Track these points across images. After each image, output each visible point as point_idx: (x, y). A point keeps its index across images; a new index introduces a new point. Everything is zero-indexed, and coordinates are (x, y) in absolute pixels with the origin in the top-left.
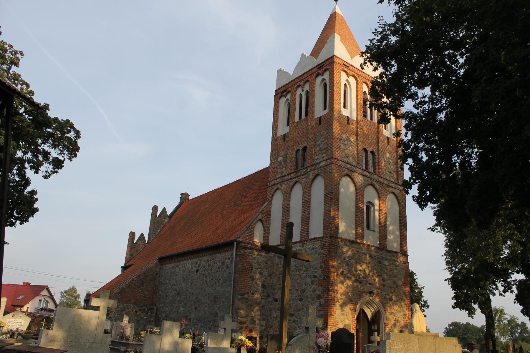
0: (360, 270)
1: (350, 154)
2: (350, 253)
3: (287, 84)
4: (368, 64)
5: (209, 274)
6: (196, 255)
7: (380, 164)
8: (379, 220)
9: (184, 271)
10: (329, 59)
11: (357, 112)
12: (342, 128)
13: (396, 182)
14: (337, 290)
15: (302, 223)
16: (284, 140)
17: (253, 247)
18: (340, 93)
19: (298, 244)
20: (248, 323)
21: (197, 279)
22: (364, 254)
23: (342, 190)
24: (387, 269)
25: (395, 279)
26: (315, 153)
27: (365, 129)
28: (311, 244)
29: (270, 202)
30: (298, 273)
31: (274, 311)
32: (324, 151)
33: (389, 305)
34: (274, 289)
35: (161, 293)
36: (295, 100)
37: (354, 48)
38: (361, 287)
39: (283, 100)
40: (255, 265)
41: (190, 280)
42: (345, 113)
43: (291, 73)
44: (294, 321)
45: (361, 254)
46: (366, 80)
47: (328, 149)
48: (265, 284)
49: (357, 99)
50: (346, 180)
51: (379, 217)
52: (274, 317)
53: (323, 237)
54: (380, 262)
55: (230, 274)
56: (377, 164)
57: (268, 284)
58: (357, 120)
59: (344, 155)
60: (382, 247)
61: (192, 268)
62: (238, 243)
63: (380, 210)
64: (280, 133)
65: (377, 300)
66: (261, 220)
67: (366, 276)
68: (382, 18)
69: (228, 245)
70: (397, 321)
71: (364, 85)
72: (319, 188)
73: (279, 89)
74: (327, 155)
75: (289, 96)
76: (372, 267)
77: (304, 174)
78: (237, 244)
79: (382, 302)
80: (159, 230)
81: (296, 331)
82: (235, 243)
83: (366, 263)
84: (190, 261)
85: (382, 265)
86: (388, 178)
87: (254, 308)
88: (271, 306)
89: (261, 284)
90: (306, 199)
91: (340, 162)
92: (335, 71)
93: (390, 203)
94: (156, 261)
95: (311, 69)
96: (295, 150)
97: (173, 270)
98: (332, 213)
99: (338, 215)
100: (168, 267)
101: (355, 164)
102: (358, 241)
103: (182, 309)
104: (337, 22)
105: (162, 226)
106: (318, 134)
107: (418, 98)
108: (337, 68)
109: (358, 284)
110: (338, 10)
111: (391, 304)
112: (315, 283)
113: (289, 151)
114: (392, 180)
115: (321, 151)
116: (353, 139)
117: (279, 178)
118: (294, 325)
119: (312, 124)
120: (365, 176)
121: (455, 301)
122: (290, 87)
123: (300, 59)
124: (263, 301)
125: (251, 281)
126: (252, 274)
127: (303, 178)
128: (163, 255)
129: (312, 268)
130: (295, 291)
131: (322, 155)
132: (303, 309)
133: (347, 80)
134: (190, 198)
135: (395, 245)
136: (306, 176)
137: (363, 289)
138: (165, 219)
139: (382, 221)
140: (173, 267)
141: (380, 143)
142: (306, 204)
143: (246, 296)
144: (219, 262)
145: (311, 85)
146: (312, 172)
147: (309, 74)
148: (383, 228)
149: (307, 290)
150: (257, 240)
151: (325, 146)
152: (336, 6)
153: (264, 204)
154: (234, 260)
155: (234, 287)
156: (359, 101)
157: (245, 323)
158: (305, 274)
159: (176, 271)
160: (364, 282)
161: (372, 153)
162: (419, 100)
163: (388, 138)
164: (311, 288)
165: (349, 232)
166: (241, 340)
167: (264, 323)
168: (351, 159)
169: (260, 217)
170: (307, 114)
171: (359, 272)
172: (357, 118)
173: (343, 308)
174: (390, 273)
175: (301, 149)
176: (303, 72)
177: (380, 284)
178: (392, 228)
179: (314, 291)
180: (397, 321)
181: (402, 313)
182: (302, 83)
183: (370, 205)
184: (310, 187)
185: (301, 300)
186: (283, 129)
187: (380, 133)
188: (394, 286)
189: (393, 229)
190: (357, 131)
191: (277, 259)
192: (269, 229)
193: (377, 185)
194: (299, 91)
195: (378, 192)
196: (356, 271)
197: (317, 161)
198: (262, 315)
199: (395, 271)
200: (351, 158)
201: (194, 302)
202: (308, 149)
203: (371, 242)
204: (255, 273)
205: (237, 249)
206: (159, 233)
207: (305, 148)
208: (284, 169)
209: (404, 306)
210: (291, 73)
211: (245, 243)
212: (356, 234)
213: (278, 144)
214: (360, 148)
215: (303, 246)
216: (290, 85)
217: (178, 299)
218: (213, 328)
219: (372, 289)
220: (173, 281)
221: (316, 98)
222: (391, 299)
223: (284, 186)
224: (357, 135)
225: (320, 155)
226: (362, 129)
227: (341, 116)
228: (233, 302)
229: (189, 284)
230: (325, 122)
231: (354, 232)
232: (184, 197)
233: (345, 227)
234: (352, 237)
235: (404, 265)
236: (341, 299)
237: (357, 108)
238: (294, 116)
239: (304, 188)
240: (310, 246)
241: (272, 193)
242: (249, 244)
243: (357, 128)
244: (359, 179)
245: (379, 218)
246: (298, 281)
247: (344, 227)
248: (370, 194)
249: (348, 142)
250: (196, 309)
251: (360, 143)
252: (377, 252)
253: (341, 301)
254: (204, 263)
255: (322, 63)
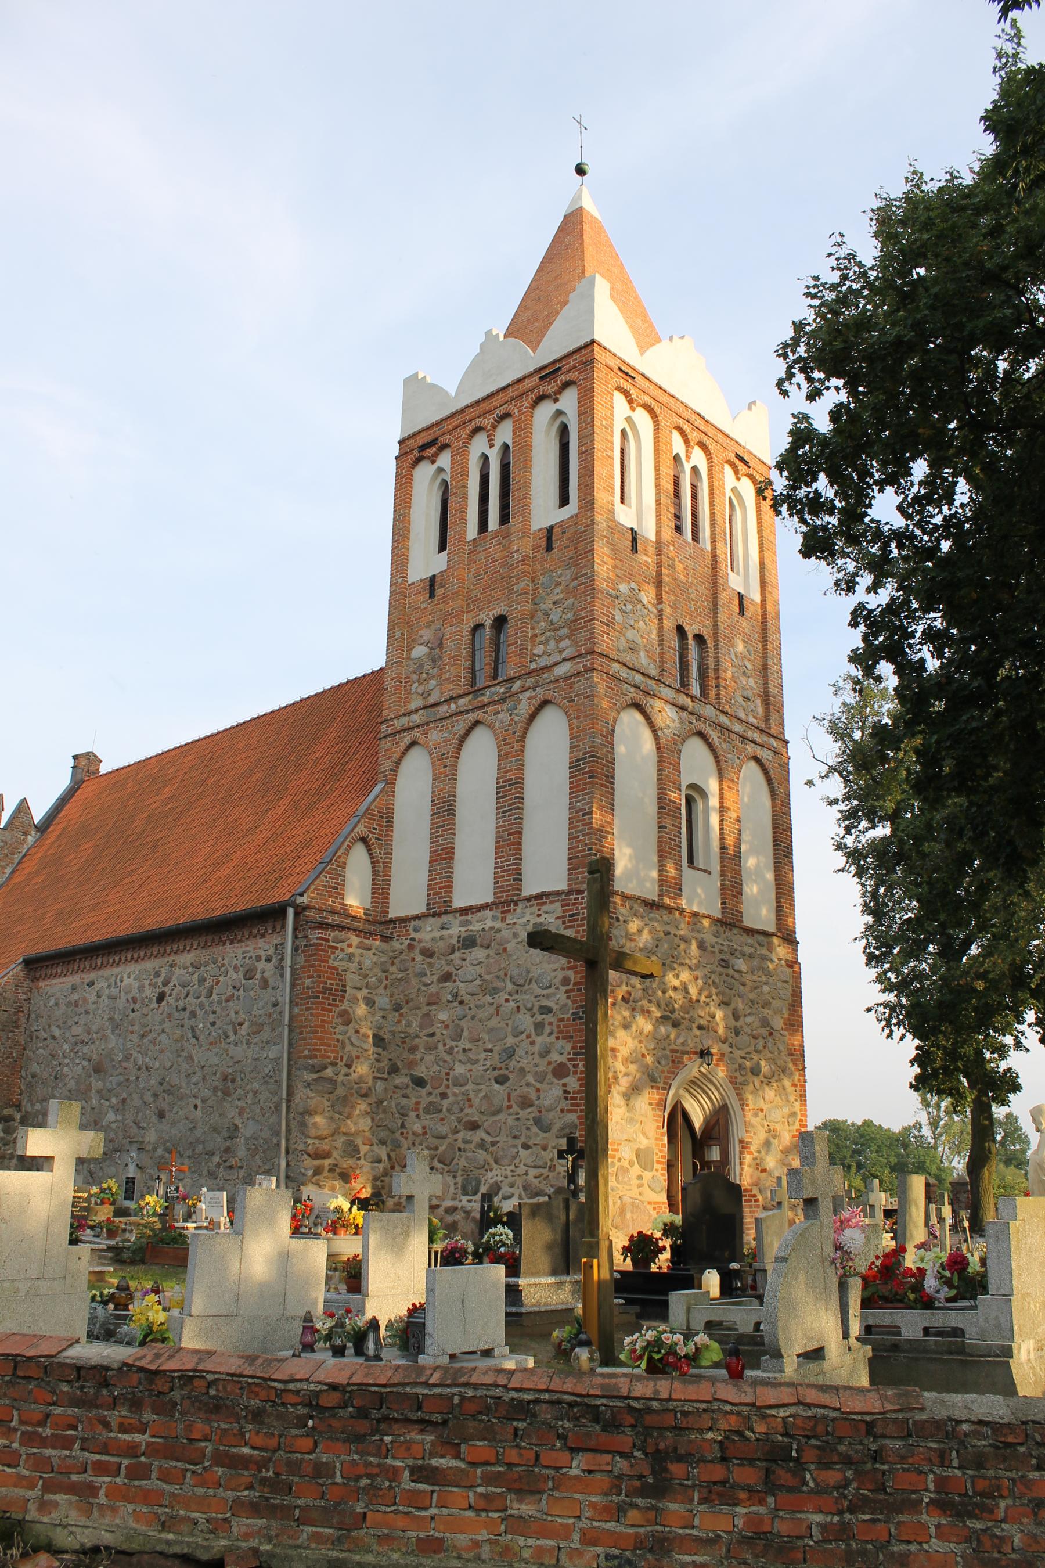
0: (675, 989)
1: (639, 640)
2: (645, 937)
3: (438, 424)
4: (800, 378)
5: (201, 1006)
6: (155, 950)
7: (722, 674)
8: (722, 839)
9: (113, 998)
10: (578, 350)
11: (658, 515)
12: (619, 564)
13: (762, 726)
14: (613, 1050)
15: (498, 848)
16: (432, 595)
17: (345, 923)
18: (612, 458)
19: (488, 913)
20: (335, 1154)
21: (162, 1022)
22: (683, 939)
23: (620, 749)
24: (744, 985)
25: (766, 1011)
26: (535, 635)
27: (679, 567)
28: (528, 911)
29: (391, 783)
30: (489, 999)
31: (413, 1114)
32: (565, 631)
33: (751, 1087)
34: (413, 1049)
35: (35, 1068)
36: (462, 473)
37: (639, 321)
38: (677, 1037)
39: (424, 473)
40: (352, 979)
41: (136, 1028)
42: (626, 517)
43: (452, 391)
44: (482, 1145)
45: (677, 940)
46: (681, 422)
47: (580, 624)
48: (381, 1033)
49: (658, 478)
50: (630, 722)
51: (721, 829)
52: (414, 1134)
53: (570, 892)
54: (725, 963)
55: (275, 1005)
56: (711, 673)
57: (393, 1033)
58: (659, 541)
59: (623, 644)
60: (730, 920)
61: (141, 989)
62: (300, 910)
63: (722, 810)
64: (419, 571)
65: (721, 1073)
66: (364, 840)
67: (692, 1004)
68: (839, 239)
69: (269, 916)
70: (772, 1133)
71: (676, 436)
72: (550, 743)
73: (410, 437)
74: (576, 643)
75: (444, 460)
76: (706, 977)
77: (503, 700)
78: (297, 914)
79: (733, 1081)
80: (8, 871)
81: (490, 1174)
82: (291, 911)
83: (690, 968)
84: (134, 968)
85: (731, 972)
86: (742, 716)
87: (353, 1107)
88: (404, 1102)
89: (370, 1033)
90: (508, 776)
91: (616, 666)
92: (597, 390)
93: (748, 789)
94: (16, 969)
95: (519, 381)
96: (467, 628)
97: (76, 997)
98: (597, 817)
99: (611, 824)
100: (58, 986)
101: (653, 672)
102: (667, 901)
103: (111, 1116)
104: (587, 238)
105: (17, 858)
106: (543, 579)
107: (912, 485)
108: (603, 381)
109: (670, 1028)
110: (588, 204)
111: (757, 1084)
112: (547, 1029)
113: (449, 630)
114: (752, 720)
115: (556, 630)
116: (647, 596)
117: (417, 711)
118: (481, 1155)
119: (522, 547)
120: (683, 708)
121: (917, 1070)
122: (450, 432)
123: (482, 346)
124: (380, 1086)
125: (341, 1028)
126: (345, 1006)
127: (496, 713)
128: (41, 948)
129: (534, 985)
130: (483, 1055)
131: (558, 642)
132: (509, 1107)
133: (629, 419)
134: (104, 769)
135: (764, 911)
136: (508, 704)
137: (683, 1044)
138: (25, 834)
139: (730, 841)
140: (74, 988)
141: (720, 610)
142: (510, 792)
143: (329, 1072)
144: (236, 969)
145: (520, 429)
146: (528, 694)
147: (511, 393)
148: (731, 861)
149: (520, 1052)
150: (356, 900)
151: (570, 616)
152: (580, 191)
153: (373, 787)
154: (288, 961)
155: (290, 1045)
156: (663, 482)
157: (327, 1155)
158: (512, 1004)
159: (85, 1000)
160: (686, 1023)
161: (699, 638)
162: (915, 489)
163: (741, 597)
164: (533, 1043)
165: (642, 874)
166: (338, 1209)
167: (383, 1152)
168: (643, 660)
169: (361, 829)
170: (505, 518)
171: (671, 993)
172: (658, 532)
173: (632, 1103)
174: (752, 996)
175: (488, 622)
176: (493, 388)
177: (726, 1027)
178: (756, 863)
179: (545, 1053)
180: (772, 1133)
181: (786, 1111)
182: (488, 421)
183: (696, 793)
184: (523, 738)
185: (501, 1080)
186: (426, 561)
187: (720, 581)
188: (764, 1032)
189: (758, 865)
190: (659, 574)
191: (419, 958)
192: (387, 865)
193: (714, 736)
194: (479, 445)
195: (716, 757)
196: (664, 992)
197: (542, 662)
198: (377, 1126)
199: (766, 989)
200: (642, 654)
201: (155, 1095)
202: (511, 623)
203: (700, 904)
204: (355, 1000)
205: (295, 929)
206: (9, 879)
207: (500, 621)
208: (433, 682)
209: (790, 1090)
210: (452, 391)
211: (320, 910)
212: (662, 880)
213: (411, 605)
214: (669, 624)
215: (503, 919)
216: (447, 426)
217: (97, 1084)
218: (222, 1172)
219: (707, 1043)
220: (77, 1030)
221: (535, 470)
222: (755, 1071)
223: (435, 736)
224: (659, 584)
225: (552, 644)
226: (672, 567)
227: (615, 527)
228: (290, 1093)
229: (135, 1038)
230: (566, 542)
231: (654, 874)
232: (85, 765)
233: (630, 859)
234: (650, 890)
235: (788, 970)
236: (626, 1074)
237: (658, 503)
238: (463, 521)
239: (502, 742)
240: (528, 917)
241: (396, 756)
242: (333, 912)
243: (659, 564)
244: (667, 716)
245: (721, 834)
246: (493, 1023)
247: (632, 865)
248: (696, 763)
249: (635, 605)
250: (161, 1115)
251: (667, 610)
252: (716, 935)
253: (624, 1082)
254: (182, 971)
255: (555, 362)
